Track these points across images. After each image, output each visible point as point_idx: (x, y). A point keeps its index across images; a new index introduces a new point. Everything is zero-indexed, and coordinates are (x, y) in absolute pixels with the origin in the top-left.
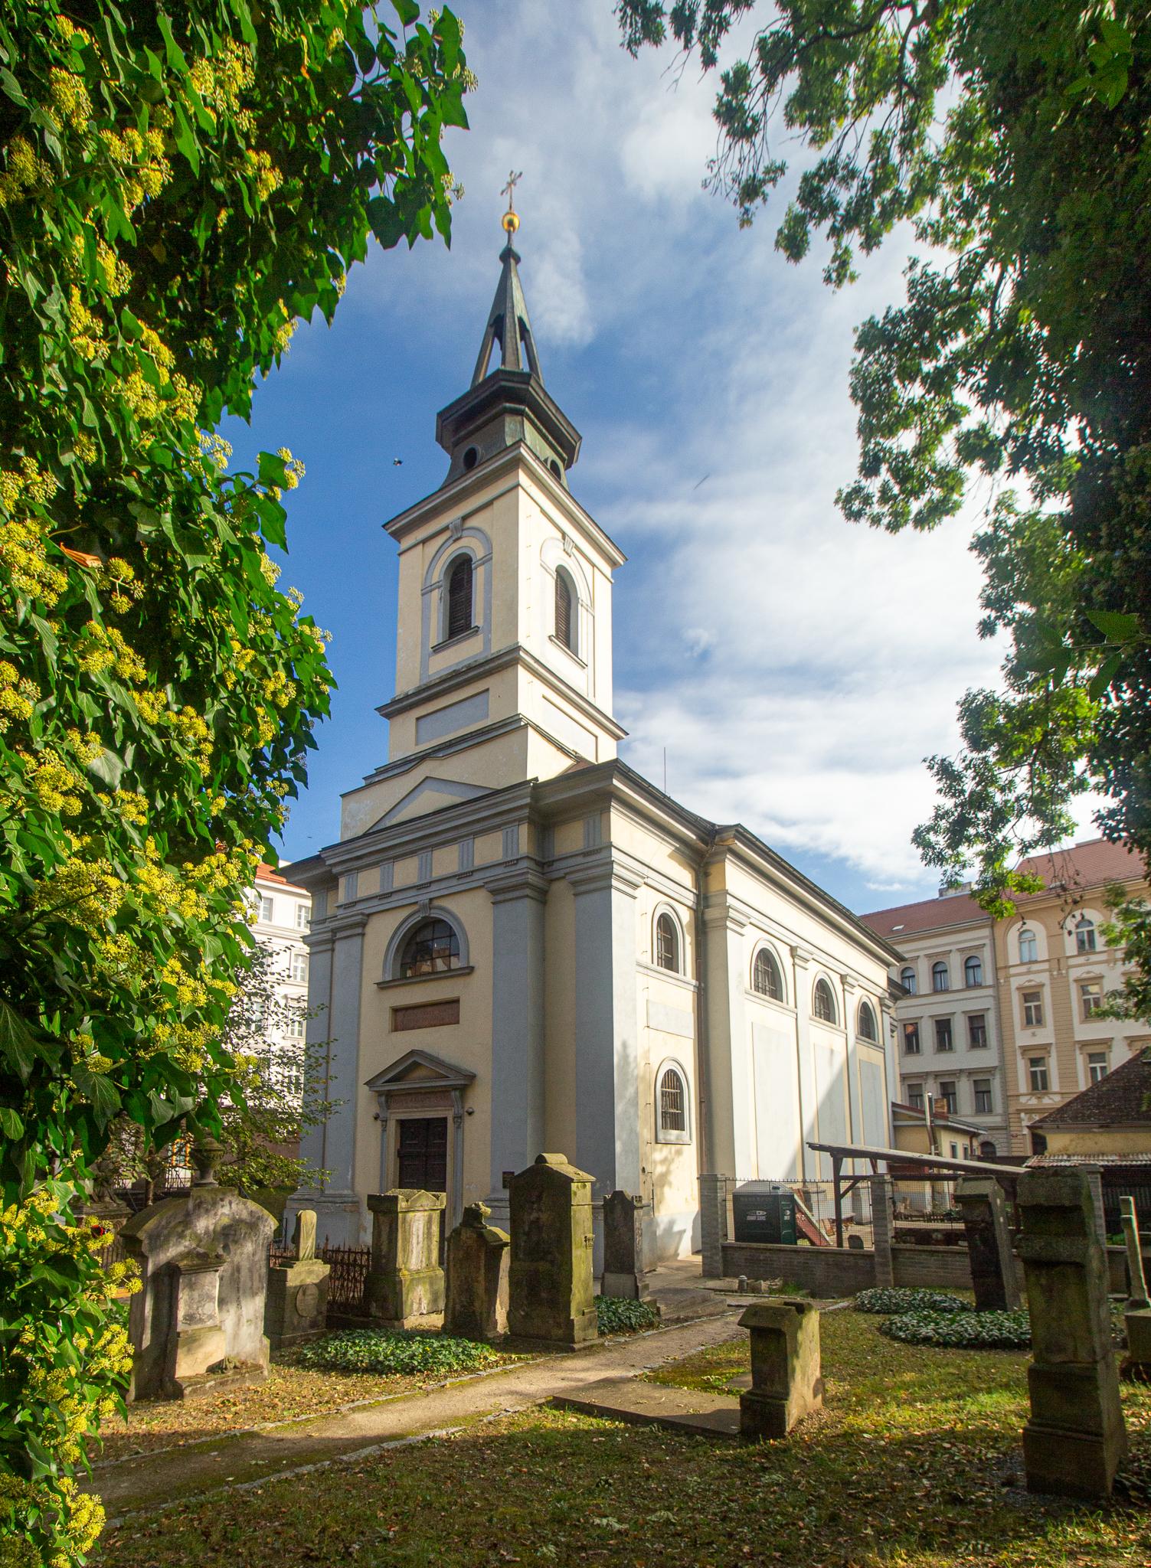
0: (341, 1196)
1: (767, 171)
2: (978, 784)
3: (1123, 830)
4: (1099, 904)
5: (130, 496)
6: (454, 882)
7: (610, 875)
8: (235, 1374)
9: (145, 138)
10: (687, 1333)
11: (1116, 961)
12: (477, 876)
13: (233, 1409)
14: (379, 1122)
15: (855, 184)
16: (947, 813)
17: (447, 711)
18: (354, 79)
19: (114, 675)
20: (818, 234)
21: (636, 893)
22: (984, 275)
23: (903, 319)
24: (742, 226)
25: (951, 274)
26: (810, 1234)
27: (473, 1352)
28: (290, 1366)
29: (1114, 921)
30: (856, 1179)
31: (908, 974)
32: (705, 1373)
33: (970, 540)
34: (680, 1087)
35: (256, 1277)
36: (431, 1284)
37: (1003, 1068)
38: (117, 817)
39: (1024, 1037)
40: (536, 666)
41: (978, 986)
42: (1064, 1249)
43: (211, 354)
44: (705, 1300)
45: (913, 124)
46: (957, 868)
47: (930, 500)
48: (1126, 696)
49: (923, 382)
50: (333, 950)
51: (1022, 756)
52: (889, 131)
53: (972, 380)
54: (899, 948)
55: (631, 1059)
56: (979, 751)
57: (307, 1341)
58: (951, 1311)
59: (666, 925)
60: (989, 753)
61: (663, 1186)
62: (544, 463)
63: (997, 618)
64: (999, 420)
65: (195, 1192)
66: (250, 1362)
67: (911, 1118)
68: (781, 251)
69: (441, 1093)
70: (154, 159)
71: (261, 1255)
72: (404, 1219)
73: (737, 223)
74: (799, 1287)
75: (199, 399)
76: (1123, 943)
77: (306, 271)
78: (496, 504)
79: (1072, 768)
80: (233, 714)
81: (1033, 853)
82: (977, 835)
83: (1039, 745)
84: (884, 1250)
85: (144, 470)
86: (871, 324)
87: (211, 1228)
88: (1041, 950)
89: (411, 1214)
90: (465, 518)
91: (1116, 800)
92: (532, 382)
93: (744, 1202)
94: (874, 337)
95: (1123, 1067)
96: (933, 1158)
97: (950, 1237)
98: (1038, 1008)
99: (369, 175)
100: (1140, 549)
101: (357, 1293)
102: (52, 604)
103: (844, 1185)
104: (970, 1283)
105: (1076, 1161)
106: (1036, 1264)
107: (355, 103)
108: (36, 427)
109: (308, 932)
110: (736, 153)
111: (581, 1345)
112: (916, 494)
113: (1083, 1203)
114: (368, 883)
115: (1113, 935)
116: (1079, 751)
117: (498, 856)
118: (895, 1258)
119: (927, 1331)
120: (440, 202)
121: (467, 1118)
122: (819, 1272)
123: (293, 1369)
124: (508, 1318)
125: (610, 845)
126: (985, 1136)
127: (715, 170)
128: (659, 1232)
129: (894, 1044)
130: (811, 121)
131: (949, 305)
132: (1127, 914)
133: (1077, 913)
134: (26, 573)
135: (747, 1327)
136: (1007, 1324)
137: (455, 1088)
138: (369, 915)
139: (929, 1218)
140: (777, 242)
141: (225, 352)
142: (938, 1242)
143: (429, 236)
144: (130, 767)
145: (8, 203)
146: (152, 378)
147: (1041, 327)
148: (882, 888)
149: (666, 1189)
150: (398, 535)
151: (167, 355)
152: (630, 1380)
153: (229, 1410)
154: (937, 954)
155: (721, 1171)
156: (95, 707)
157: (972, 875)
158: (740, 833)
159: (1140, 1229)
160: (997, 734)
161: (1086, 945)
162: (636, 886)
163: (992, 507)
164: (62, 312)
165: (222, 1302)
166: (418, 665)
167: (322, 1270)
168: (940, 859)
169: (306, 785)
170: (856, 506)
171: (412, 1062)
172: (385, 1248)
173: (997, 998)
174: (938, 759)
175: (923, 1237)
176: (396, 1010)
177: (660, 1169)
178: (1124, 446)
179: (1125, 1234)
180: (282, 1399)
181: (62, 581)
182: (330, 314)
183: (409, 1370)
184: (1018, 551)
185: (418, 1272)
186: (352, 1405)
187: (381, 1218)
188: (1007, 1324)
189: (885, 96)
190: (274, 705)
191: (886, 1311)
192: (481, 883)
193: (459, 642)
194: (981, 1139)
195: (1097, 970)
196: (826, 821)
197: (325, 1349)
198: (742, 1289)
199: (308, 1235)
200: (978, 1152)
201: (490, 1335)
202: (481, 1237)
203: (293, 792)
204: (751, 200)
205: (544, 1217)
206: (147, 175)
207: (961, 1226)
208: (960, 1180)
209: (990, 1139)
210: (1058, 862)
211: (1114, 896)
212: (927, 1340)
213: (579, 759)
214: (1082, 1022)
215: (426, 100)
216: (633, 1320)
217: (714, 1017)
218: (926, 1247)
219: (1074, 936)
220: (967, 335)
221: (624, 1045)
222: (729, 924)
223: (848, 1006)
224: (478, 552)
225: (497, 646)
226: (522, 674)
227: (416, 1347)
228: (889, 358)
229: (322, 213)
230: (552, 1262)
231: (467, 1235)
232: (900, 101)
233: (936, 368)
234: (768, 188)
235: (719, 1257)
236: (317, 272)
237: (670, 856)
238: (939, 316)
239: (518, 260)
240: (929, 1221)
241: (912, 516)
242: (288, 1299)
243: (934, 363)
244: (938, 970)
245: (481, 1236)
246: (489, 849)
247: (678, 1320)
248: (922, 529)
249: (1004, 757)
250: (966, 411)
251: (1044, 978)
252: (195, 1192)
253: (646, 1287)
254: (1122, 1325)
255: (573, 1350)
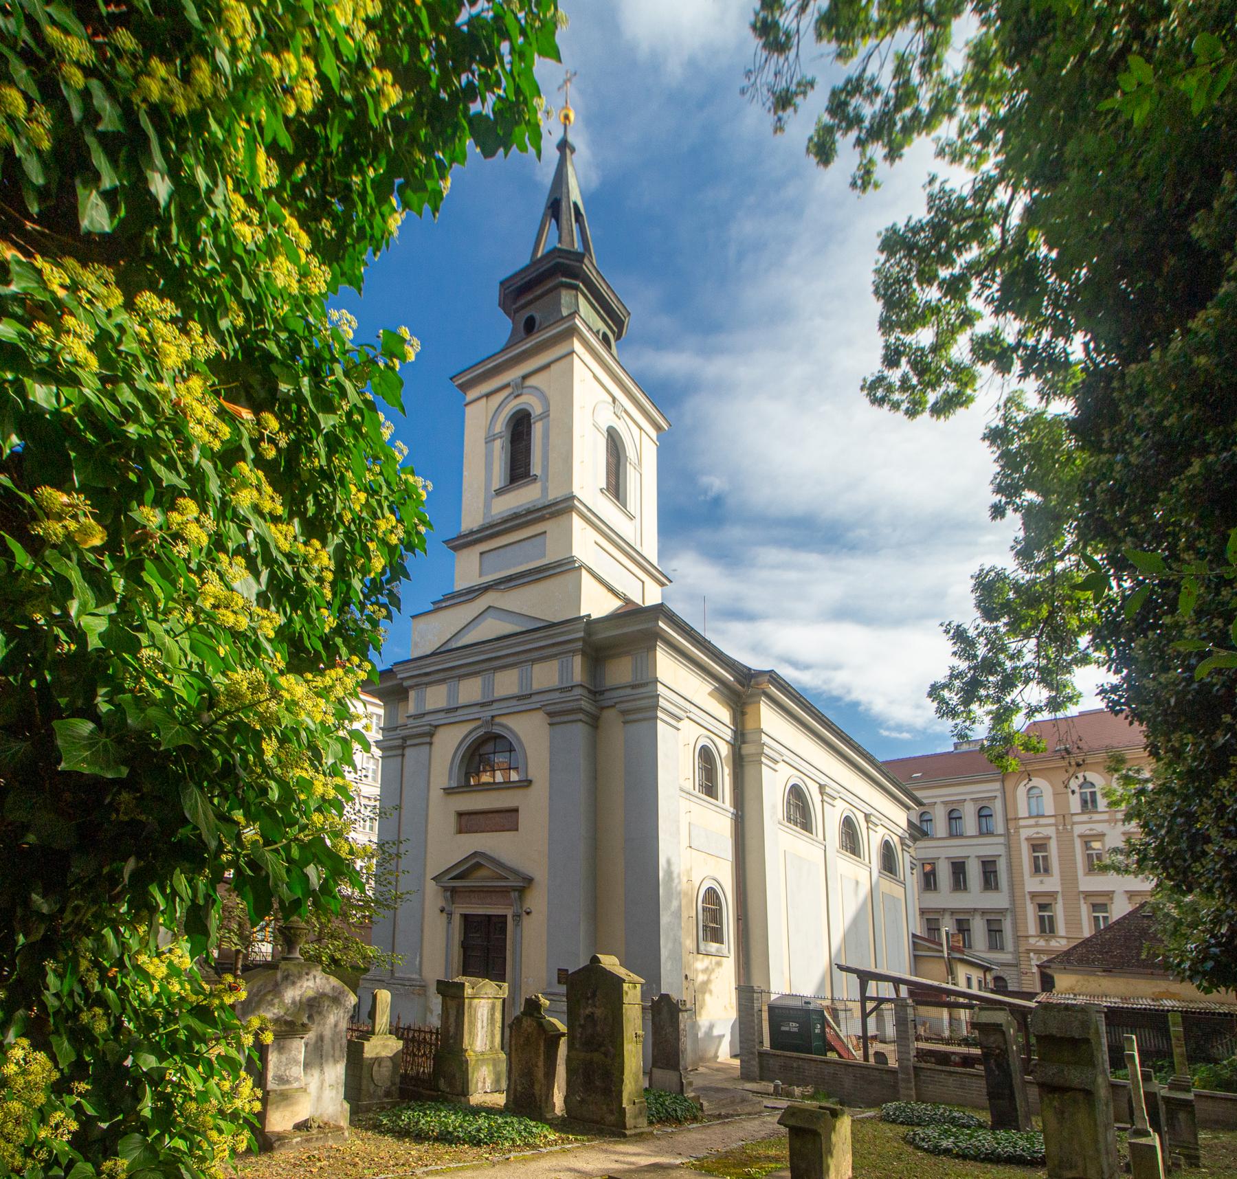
0: (409, 980)
1: (799, 84)
2: (989, 651)
3: (1123, 704)
4: (1101, 769)
5: (270, 357)
6: (514, 702)
7: (656, 706)
8: (319, 1133)
9: (299, 63)
10: (728, 1129)
11: (1116, 821)
12: (534, 699)
13: (318, 1164)
14: (444, 915)
15: (879, 101)
16: (960, 673)
17: (509, 548)
18: (460, 10)
19: (256, 509)
20: (845, 142)
21: (680, 725)
22: (996, 194)
23: (922, 229)
24: (775, 132)
25: (966, 191)
26: (838, 1048)
27: (534, 1130)
28: (367, 1129)
29: (1114, 785)
30: (881, 1001)
31: (926, 818)
32: (746, 1165)
33: (982, 431)
34: (720, 904)
35: (337, 1045)
36: (494, 1066)
37: (1014, 910)
38: (254, 630)
39: (1032, 884)
40: (589, 514)
41: (990, 833)
42: (1074, 1076)
43: (329, 233)
44: (743, 1100)
45: (932, 51)
46: (967, 723)
47: (946, 393)
48: (1127, 584)
49: (940, 286)
50: (403, 755)
51: (1031, 629)
52: (910, 53)
53: (987, 293)
54: (918, 794)
55: (675, 875)
56: (991, 621)
57: (383, 1109)
58: (968, 1127)
59: (706, 757)
60: (1000, 624)
61: (704, 993)
62: (596, 333)
63: (1007, 503)
64: (1010, 329)
65: (283, 965)
66: (332, 1123)
67: (930, 949)
68: (812, 156)
69: (504, 892)
70: (307, 79)
71: (344, 1025)
72: (470, 1004)
73: (771, 130)
74: (828, 1096)
75: (329, 278)
76: (1123, 806)
77: (417, 171)
78: (553, 367)
79: (1077, 643)
80: (348, 547)
81: (1038, 717)
82: (988, 696)
83: (1046, 622)
84: (907, 1067)
85: (283, 336)
86: (893, 230)
87: (298, 998)
88: (1048, 806)
89: (476, 1001)
90: (525, 377)
91: (1118, 676)
92: (586, 261)
93: (779, 1013)
94: (896, 243)
95: (1124, 918)
96: (950, 986)
97: (967, 1061)
98: (1045, 858)
99: (470, 93)
100: (1139, 455)
101: (427, 1067)
102: (216, 449)
103: (870, 1005)
104: (987, 1104)
105: (1081, 1000)
106: (1048, 1088)
107: (462, 32)
108: (197, 294)
109: (380, 737)
110: (771, 67)
111: (633, 1132)
112: (933, 386)
113: (1092, 1036)
114: (436, 697)
115: (1114, 798)
116: (1082, 628)
117: (554, 682)
118: (916, 1075)
119: (945, 1144)
120: (532, 121)
121: (525, 917)
122: (848, 1082)
123: (370, 1133)
124: (565, 1102)
125: (656, 681)
126: (998, 971)
127: (752, 80)
128: (700, 1035)
129: (913, 880)
130: (839, 38)
131: (964, 220)
132: (1127, 780)
133: (1080, 775)
134: (200, 423)
135: (786, 1126)
136: (1020, 1143)
137: (514, 889)
138: (436, 727)
139: (948, 1042)
140: (808, 148)
141: (343, 232)
142: (956, 1065)
143: (523, 149)
144: (264, 588)
145: (188, 111)
146: (293, 259)
147: (1050, 250)
148: (894, 735)
149: (707, 996)
150: (464, 387)
151: (305, 241)
152: (678, 1167)
153: (314, 1165)
154: (953, 802)
155: (757, 983)
156: (240, 535)
157: (981, 730)
158: (773, 678)
159: (1142, 1065)
160: (1007, 607)
161: (1089, 803)
162: (679, 719)
163: (1001, 403)
164: (225, 202)
165: (307, 1066)
166: (481, 505)
167: (396, 1045)
168: (953, 713)
169: (399, 610)
170: (880, 393)
171: (474, 864)
172: (452, 1030)
173: (1008, 847)
174: (954, 624)
175: (943, 1058)
176: (460, 814)
177: (701, 978)
178: (1126, 360)
179: (1129, 1071)
180: (362, 1159)
181: (225, 431)
182: (436, 209)
183: (477, 1142)
184: (1026, 447)
185: (482, 1053)
186: (425, 1169)
187: (450, 1002)
188: (1020, 1143)
189: (908, 21)
190: (384, 542)
191: (908, 1122)
192: (538, 705)
193: (519, 487)
194: (994, 973)
195: (1099, 828)
196: (837, 667)
197: (399, 1117)
198: (777, 1093)
199: (383, 1013)
200: (991, 985)
201: (549, 1116)
202: (542, 1027)
203: (389, 616)
204: (784, 108)
205: (599, 1012)
206: (301, 94)
207: (977, 1051)
208: (976, 1009)
209: (1001, 974)
210: (1063, 728)
211: (1115, 763)
212: (947, 1151)
213: (627, 601)
214: (1086, 874)
215: (523, 32)
216: (679, 1113)
217: (751, 843)
218: (944, 1068)
219: (1077, 796)
220: (980, 247)
221: (669, 862)
222: (763, 759)
223: (872, 841)
224: (537, 409)
225: (554, 494)
226: (576, 520)
227: (482, 1121)
228: (909, 263)
229: (430, 122)
230: (606, 1055)
231: (527, 1023)
232: (920, 27)
233: (952, 275)
234: (799, 100)
235: (755, 1062)
236: (428, 173)
237: (710, 694)
238: (955, 228)
239: (573, 150)
240: (948, 1044)
241: (929, 405)
242: (365, 1070)
243: (950, 270)
244: (953, 817)
245: (540, 1025)
246: (545, 675)
247: (719, 1116)
248: (938, 417)
249: (1013, 628)
250: (980, 316)
251: (1051, 831)
252: (283, 965)
253: (690, 1084)
254: (1124, 1150)
255: (625, 1136)
